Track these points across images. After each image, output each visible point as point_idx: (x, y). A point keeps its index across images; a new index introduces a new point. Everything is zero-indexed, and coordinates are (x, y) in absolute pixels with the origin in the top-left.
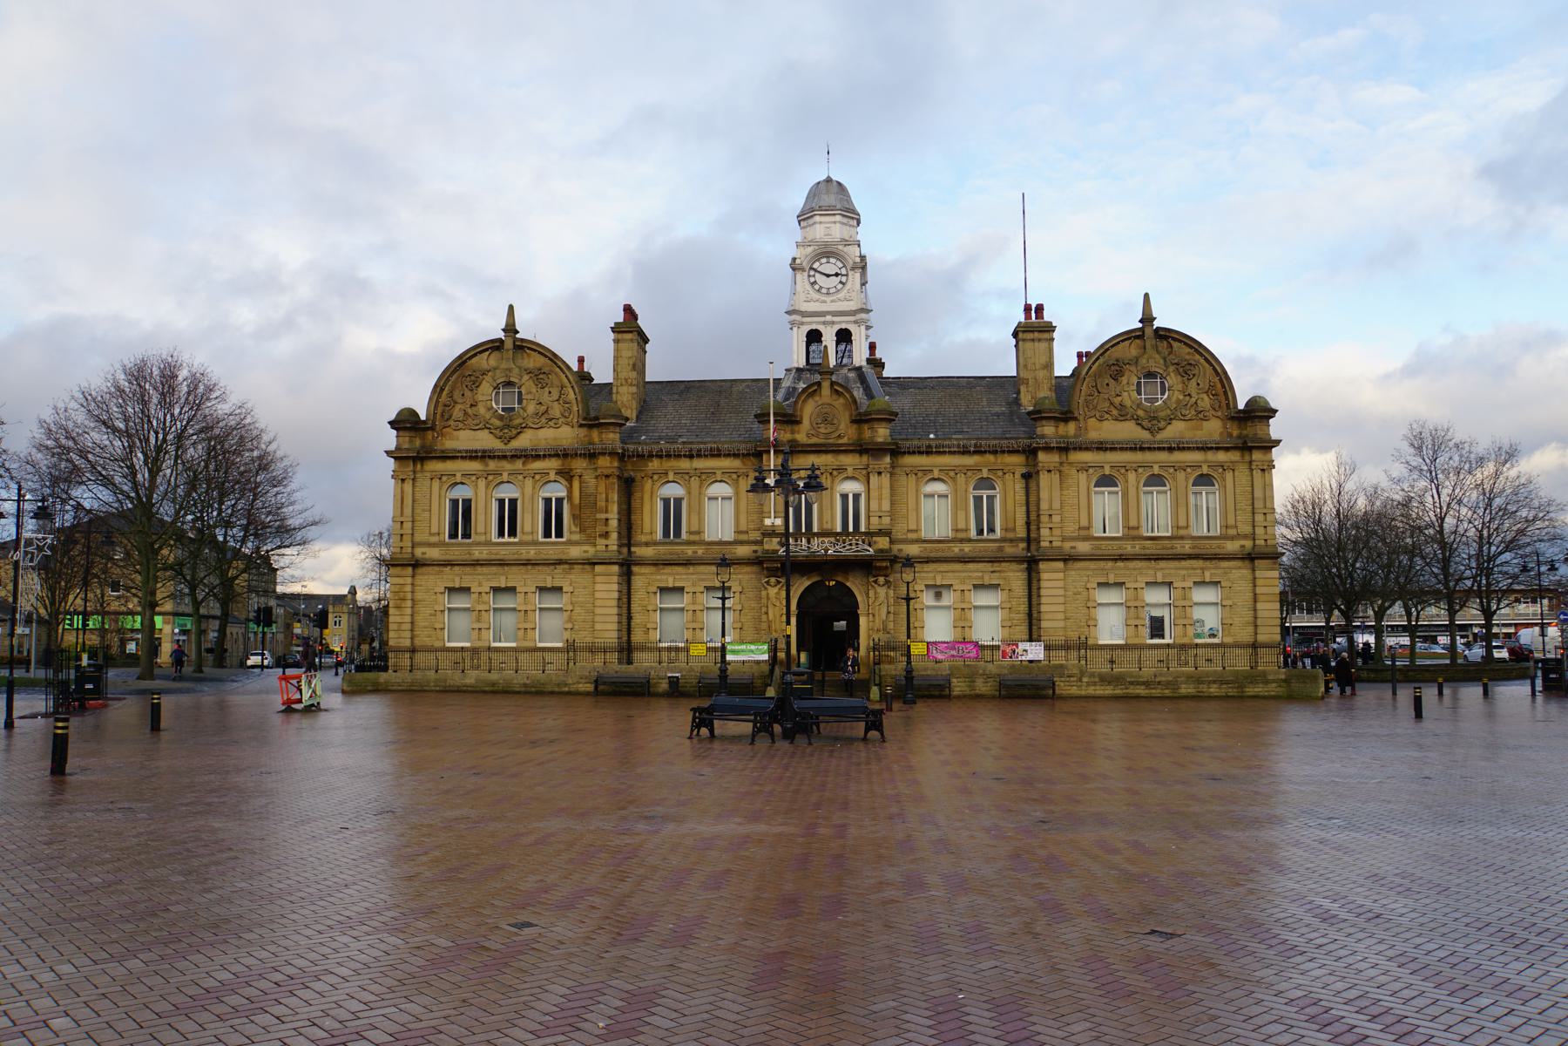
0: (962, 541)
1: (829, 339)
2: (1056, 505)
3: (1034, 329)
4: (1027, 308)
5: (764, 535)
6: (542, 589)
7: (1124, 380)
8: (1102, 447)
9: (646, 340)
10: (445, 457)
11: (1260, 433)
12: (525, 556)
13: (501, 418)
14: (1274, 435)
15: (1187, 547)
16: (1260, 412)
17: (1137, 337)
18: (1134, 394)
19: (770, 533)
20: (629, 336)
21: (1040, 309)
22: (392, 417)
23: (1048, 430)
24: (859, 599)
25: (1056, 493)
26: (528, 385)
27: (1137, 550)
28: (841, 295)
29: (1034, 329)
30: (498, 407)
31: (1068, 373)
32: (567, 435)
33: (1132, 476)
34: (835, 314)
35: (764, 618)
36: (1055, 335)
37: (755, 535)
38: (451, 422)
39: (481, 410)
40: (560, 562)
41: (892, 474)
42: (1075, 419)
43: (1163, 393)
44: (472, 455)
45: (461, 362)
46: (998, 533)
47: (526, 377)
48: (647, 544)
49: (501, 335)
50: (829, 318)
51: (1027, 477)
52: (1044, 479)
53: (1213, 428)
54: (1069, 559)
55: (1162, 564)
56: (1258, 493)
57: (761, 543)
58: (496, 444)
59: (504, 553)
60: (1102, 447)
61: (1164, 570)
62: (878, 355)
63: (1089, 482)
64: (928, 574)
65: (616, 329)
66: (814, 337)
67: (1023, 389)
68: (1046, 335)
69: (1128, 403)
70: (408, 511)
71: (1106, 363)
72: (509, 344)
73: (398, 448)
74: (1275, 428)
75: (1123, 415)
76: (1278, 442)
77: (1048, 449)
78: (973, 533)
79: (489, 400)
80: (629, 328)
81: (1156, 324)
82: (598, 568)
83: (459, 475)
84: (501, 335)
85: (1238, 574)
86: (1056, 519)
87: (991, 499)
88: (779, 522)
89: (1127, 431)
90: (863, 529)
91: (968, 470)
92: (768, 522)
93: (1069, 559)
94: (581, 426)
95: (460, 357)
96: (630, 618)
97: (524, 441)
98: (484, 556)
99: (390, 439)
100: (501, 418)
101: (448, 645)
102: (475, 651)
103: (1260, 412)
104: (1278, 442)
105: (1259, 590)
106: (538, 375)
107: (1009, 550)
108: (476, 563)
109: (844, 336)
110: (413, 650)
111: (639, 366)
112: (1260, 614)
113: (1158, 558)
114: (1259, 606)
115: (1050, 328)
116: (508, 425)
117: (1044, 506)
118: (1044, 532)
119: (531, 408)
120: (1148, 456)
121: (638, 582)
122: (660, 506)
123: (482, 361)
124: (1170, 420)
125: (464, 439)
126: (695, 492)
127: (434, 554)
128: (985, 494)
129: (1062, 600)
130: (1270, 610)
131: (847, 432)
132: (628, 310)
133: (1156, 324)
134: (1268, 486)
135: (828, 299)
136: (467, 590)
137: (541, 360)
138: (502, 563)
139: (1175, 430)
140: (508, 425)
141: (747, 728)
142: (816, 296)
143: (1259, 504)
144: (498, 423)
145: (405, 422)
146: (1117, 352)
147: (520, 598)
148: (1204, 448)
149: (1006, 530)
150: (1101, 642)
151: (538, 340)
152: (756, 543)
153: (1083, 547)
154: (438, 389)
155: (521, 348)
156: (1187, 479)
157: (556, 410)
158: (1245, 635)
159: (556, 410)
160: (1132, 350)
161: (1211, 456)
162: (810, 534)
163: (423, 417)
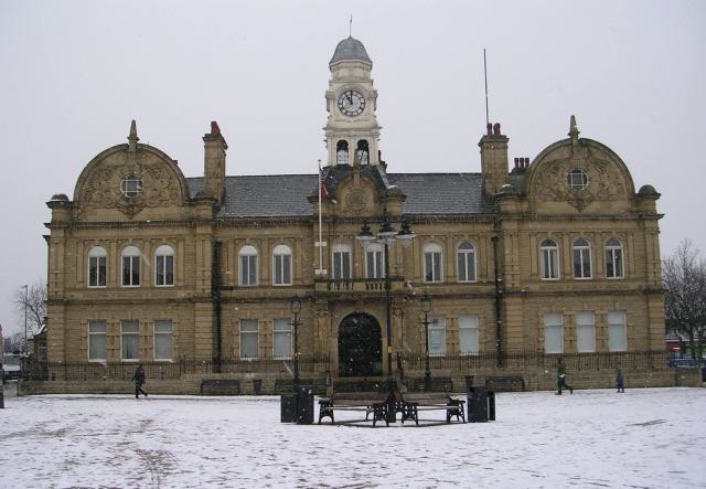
0: (265, 287)
1: (353, 145)
2: (516, 259)
3: (494, 140)
4: (489, 126)
5: (317, 281)
6: (158, 322)
7: (560, 173)
8: (546, 218)
9: (226, 147)
11: (650, 208)
13: (127, 200)
14: (659, 212)
16: (650, 194)
17: (567, 145)
18: (566, 184)
19: (320, 280)
20: (215, 143)
21: (498, 126)
23: (510, 206)
25: (516, 251)
26: (146, 177)
28: (359, 117)
29: (494, 140)
30: (125, 193)
31: (187, 175)
32: (174, 211)
33: (599, 238)
35: (316, 339)
37: (307, 282)
38: (92, 203)
40: (170, 301)
41: (65, 244)
42: (529, 201)
43: (585, 183)
44: (156, 224)
45: (98, 162)
48: (231, 289)
49: (127, 141)
50: (353, 133)
52: (507, 241)
54: (526, 295)
56: (650, 250)
57: (313, 286)
58: (122, 218)
59: (128, 296)
60: (546, 218)
62: (382, 159)
63: (570, 243)
65: (207, 138)
66: (342, 146)
68: (502, 145)
69: (562, 189)
70: (61, 265)
72: (132, 149)
73: (53, 222)
74: (660, 206)
75: (559, 197)
76: (661, 216)
79: (117, 186)
80: (215, 140)
81: (580, 136)
82: (199, 305)
83: (582, 232)
84: (127, 141)
85: (638, 304)
86: (516, 268)
87: (471, 255)
88: (325, 272)
92: (317, 272)
96: (220, 340)
99: (48, 215)
100: (127, 200)
101: (90, 361)
102: (111, 365)
103: (650, 194)
104: (661, 216)
105: (652, 315)
107: (484, 289)
110: (65, 365)
111: (221, 165)
115: (505, 139)
116: (132, 204)
117: (508, 259)
118: (509, 277)
119: (149, 193)
121: (225, 314)
122: (273, 259)
124: (591, 201)
125: (103, 215)
126: (265, 250)
127: (80, 296)
128: (466, 252)
129: (521, 324)
130: (658, 328)
131: (370, 205)
132: (214, 125)
133: (580, 136)
134: (656, 246)
135: (350, 119)
136: (103, 322)
137: (154, 160)
138: (129, 303)
139: (593, 208)
140: (132, 204)
141: (442, 414)
142: (344, 117)
143: (650, 257)
144: (123, 203)
145: (58, 203)
146: (110, 161)
147: (109, 327)
148: (613, 219)
149: (481, 276)
150: (581, 351)
152: (308, 286)
154: (82, 179)
155: (140, 151)
156: (602, 240)
157: (166, 194)
159: (166, 194)
161: (618, 225)
162: (347, 281)
163: (71, 199)
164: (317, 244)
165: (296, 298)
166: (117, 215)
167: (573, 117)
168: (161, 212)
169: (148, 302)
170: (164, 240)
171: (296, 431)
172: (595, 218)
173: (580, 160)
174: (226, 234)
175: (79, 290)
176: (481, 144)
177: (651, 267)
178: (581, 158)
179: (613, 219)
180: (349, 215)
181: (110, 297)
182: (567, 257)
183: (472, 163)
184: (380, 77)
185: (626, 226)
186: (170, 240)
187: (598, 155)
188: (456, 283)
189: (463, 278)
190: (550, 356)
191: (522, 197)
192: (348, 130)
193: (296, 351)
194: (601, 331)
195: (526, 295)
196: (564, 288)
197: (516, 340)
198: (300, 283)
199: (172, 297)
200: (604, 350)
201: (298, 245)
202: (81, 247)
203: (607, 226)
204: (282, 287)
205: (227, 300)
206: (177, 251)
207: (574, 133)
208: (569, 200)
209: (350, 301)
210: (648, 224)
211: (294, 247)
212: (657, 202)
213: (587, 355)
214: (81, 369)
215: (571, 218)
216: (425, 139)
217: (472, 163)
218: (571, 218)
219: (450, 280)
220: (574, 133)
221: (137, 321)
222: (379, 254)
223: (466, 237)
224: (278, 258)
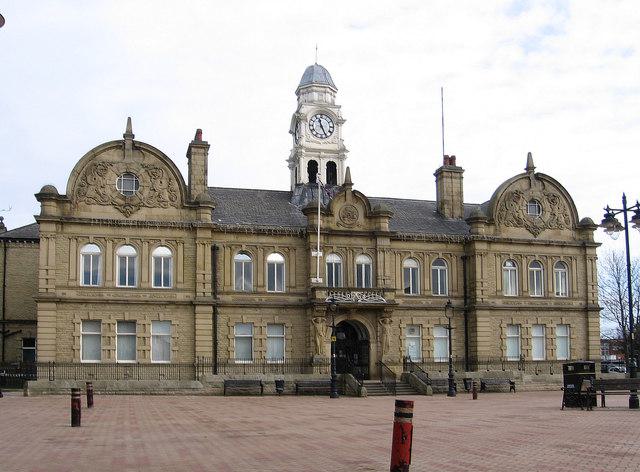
3: (449, 171)
4: (446, 157)
7: (520, 202)
8: (509, 242)
10: (83, 223)
12: (142, 298)
13: (124, 198)
14: (596, 241)
15: (552, 304)
22: (38, 191)
23: (483, 230)
24: (371, 333)
27: (148, 298)
29: (449, 171)
32: (172, 213)
34: (326, 151)
36: (464, 175)
39: (108, 191)
42: (494, 224)
45: (94, 153)
46: (172, 285)
47: (142, 171)
48: (228, 293)
51: (464, 259)
53: (567, 234)
54: (492, 309)
55: (541, 313)
59: (127, 296)
60: (509, 242)
61: (543, 317)
64: (406, 318)
67: (446, 206)
68: (202, 151)
71: (507, 196)
75: (519, 223)
77: (482, 241)
78: (81, 283)
79: (114, 182)
80: (198, 147)
89: (520, 233)
90: (364, 286)
91: (429, 253)
93: (492, 309)
94: (184, 207)
95: (92, 151)
97: (141, 215)
98: (111, 298)
101: (82, 361)
106: (152, 171)
108: (107, 302)
109: (331, 167)
112: (591, 343)
113: (243, 306)
114: (591, 338)
115: (460, 171)
116: (128, 204)
118: (478, 292)
120: (533, 249)
121: (221, 319)
123: (105, 156)
124: (544, 229)
125: (96, 212)
128: (439, 268)
131: (361, 223)
138: (127, 303)
139: (544, 235)
140: (128, 204)
142: (315, 139)
144: (122, 202)
146: (105, 156)
148: (562, 245)
150: (534, 359)
151: (500, 184)
153: (499, 303)
158: (186, 359)
160: (114, 156)
164: (314, 254)
165: (286, 307)
166: (111, 213)
167: (129, 119)
168: (158, 214)
169: (147, 303)
170: (163, 243)
171: (580, 417)
172: (548, 244)
173: (537, 191)
174: (222, 240)
175: (72, 288)
176: (436, 174)
177: (590, 287)
178: (536, 191)
179: (562, 245)
180: (342, 228)
181: (105, 296)
182: (525, 277)
183: (428, 193)
184: (345, 101)
185: (570, 251)
186: (168, 243)
187: (551, 189)
188: (265, 293)
189: (271, 287)
190: (560, 361)
191: (490, 222)
192: (320, 151)
193: (451, 353)
194: (549, 343)
195: (60, 301)
196: (565, 304)
197: (485, 349)
198: (292, 290)
199: (172, 300)
200: (552, 358)
201: (292, 254)
202: (74, 243)
203: (556, 251)
204: (276, 293)
205: (224, 305)
206: (288, 261)
207: (530, 168)
208: (527, 227)
209: (344, 309)
210: (589, 251)
211: (174, 250)
212: (594, 232)
213: (538, 362)
214: (72, 370)
215: (529, 243)
216: (389, 168)
217: (428, 193)
218: (529, 243)
219: (260, 290)
220: (530, 168)
221: (100, 321)
222: (367, 266)
223: (441, 254)
224: (271, 265)
